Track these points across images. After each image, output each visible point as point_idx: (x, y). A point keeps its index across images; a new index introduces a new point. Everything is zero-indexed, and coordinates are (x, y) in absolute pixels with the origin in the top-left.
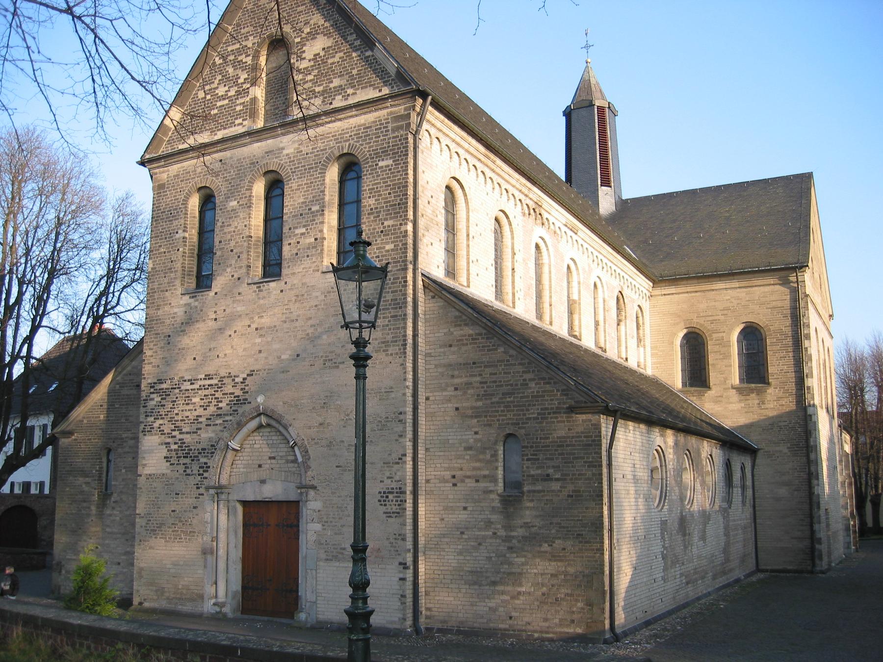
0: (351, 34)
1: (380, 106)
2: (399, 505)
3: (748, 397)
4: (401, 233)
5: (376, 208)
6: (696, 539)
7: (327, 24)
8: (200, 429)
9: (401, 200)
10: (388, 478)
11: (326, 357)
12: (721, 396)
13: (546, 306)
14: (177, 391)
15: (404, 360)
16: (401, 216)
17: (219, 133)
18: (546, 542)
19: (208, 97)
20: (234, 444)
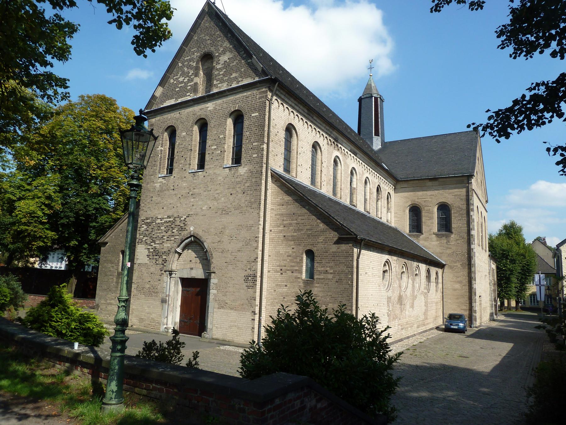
0: (242, 51)
1: (253, 87)
2: (254, 283)
3: (441, 239)
4: (261, 149)
5: (250, 137)
6: (408, 306)
7: (231, 46)
9: (261, 133)
10: (249, 269)
11: (223, 209)
12: (428, 238)
13: (339, 189)
14: (154, 223)
15: (260, 212)
16: (261, 141)
17: (179, 100)
18: (324, 304)
19: (175, 82)
20: (179, 250)
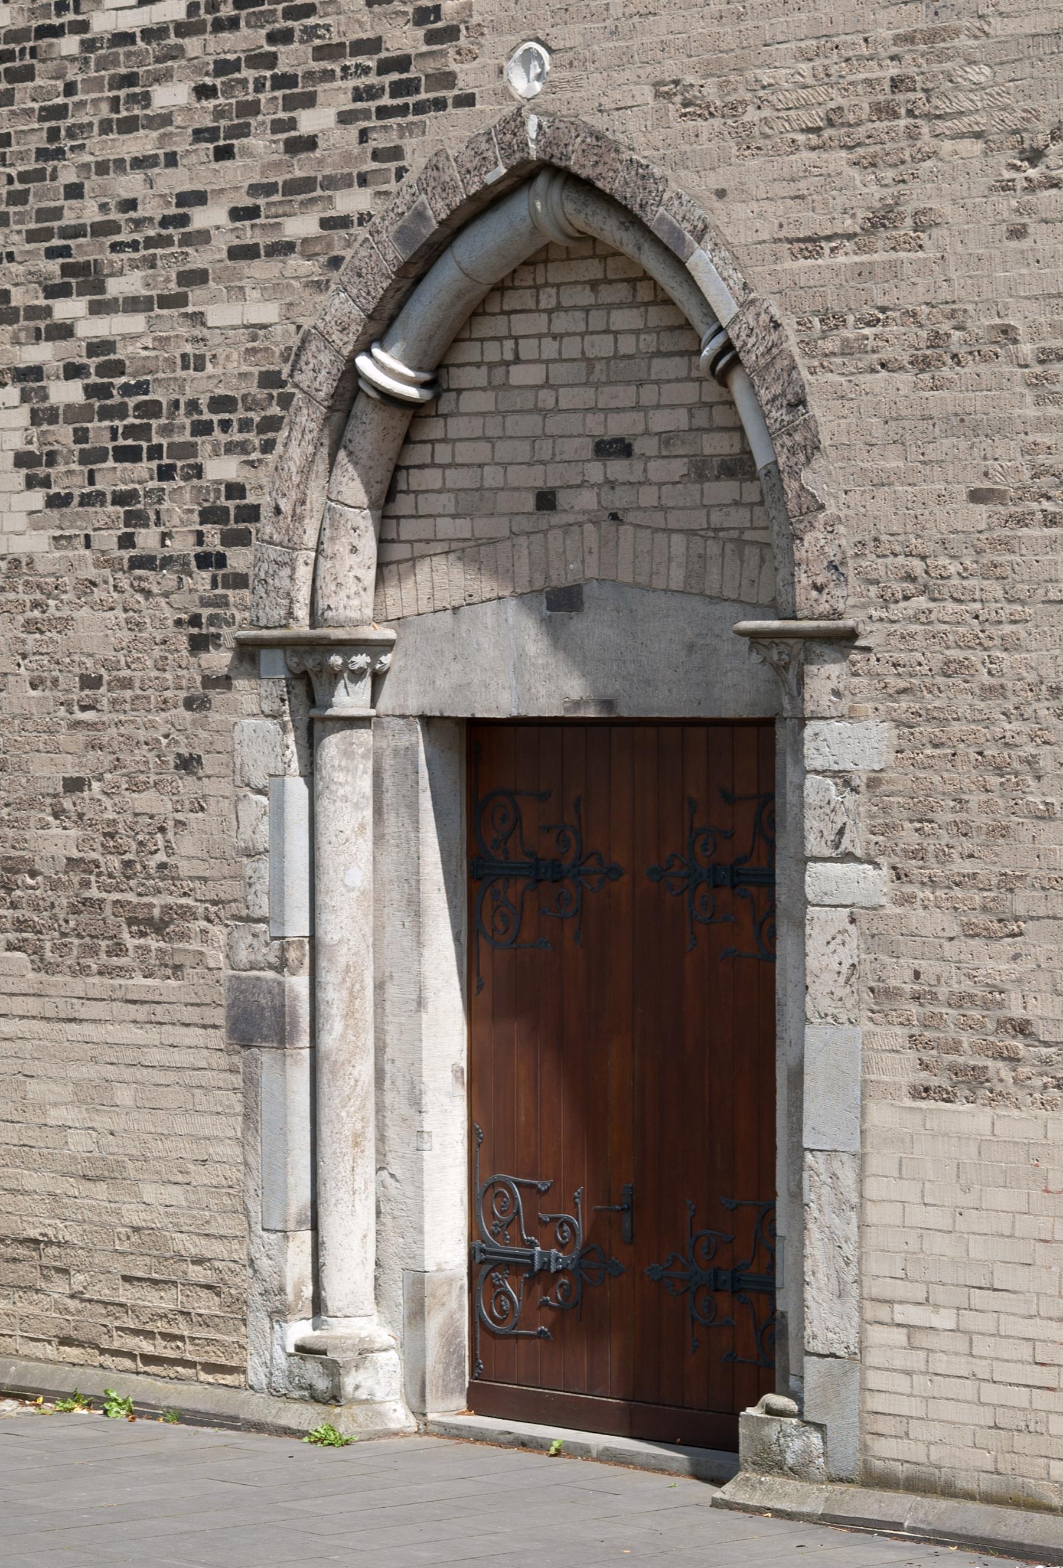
8: (198, 277)
14: (69, 45)
